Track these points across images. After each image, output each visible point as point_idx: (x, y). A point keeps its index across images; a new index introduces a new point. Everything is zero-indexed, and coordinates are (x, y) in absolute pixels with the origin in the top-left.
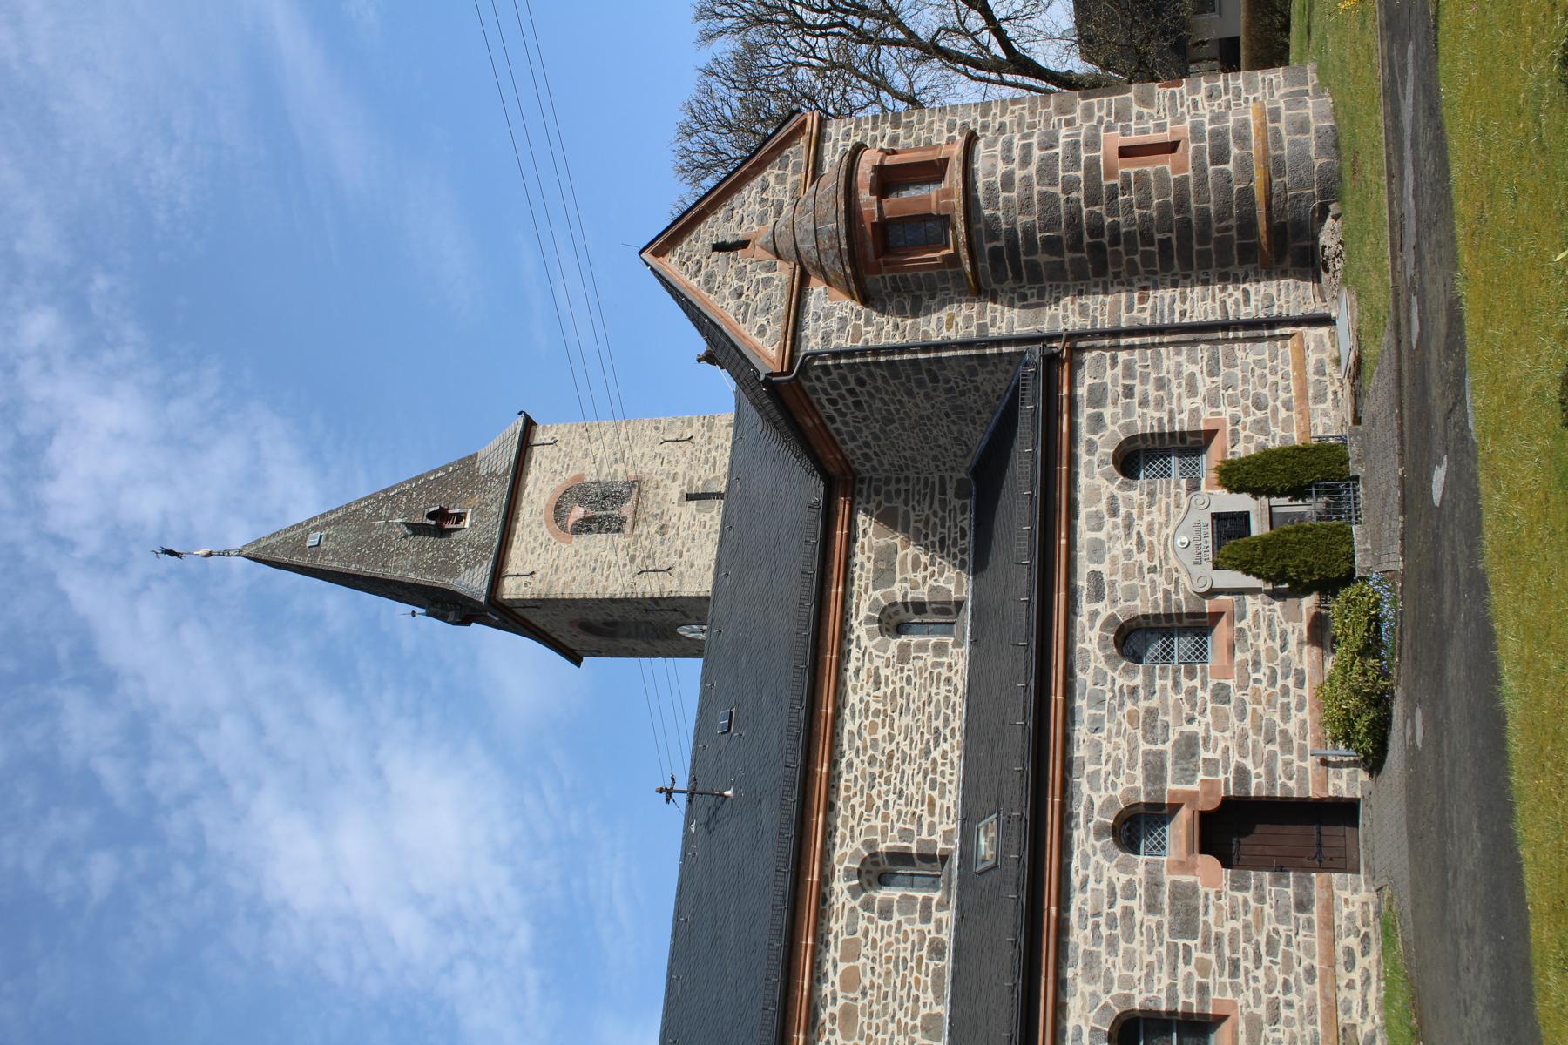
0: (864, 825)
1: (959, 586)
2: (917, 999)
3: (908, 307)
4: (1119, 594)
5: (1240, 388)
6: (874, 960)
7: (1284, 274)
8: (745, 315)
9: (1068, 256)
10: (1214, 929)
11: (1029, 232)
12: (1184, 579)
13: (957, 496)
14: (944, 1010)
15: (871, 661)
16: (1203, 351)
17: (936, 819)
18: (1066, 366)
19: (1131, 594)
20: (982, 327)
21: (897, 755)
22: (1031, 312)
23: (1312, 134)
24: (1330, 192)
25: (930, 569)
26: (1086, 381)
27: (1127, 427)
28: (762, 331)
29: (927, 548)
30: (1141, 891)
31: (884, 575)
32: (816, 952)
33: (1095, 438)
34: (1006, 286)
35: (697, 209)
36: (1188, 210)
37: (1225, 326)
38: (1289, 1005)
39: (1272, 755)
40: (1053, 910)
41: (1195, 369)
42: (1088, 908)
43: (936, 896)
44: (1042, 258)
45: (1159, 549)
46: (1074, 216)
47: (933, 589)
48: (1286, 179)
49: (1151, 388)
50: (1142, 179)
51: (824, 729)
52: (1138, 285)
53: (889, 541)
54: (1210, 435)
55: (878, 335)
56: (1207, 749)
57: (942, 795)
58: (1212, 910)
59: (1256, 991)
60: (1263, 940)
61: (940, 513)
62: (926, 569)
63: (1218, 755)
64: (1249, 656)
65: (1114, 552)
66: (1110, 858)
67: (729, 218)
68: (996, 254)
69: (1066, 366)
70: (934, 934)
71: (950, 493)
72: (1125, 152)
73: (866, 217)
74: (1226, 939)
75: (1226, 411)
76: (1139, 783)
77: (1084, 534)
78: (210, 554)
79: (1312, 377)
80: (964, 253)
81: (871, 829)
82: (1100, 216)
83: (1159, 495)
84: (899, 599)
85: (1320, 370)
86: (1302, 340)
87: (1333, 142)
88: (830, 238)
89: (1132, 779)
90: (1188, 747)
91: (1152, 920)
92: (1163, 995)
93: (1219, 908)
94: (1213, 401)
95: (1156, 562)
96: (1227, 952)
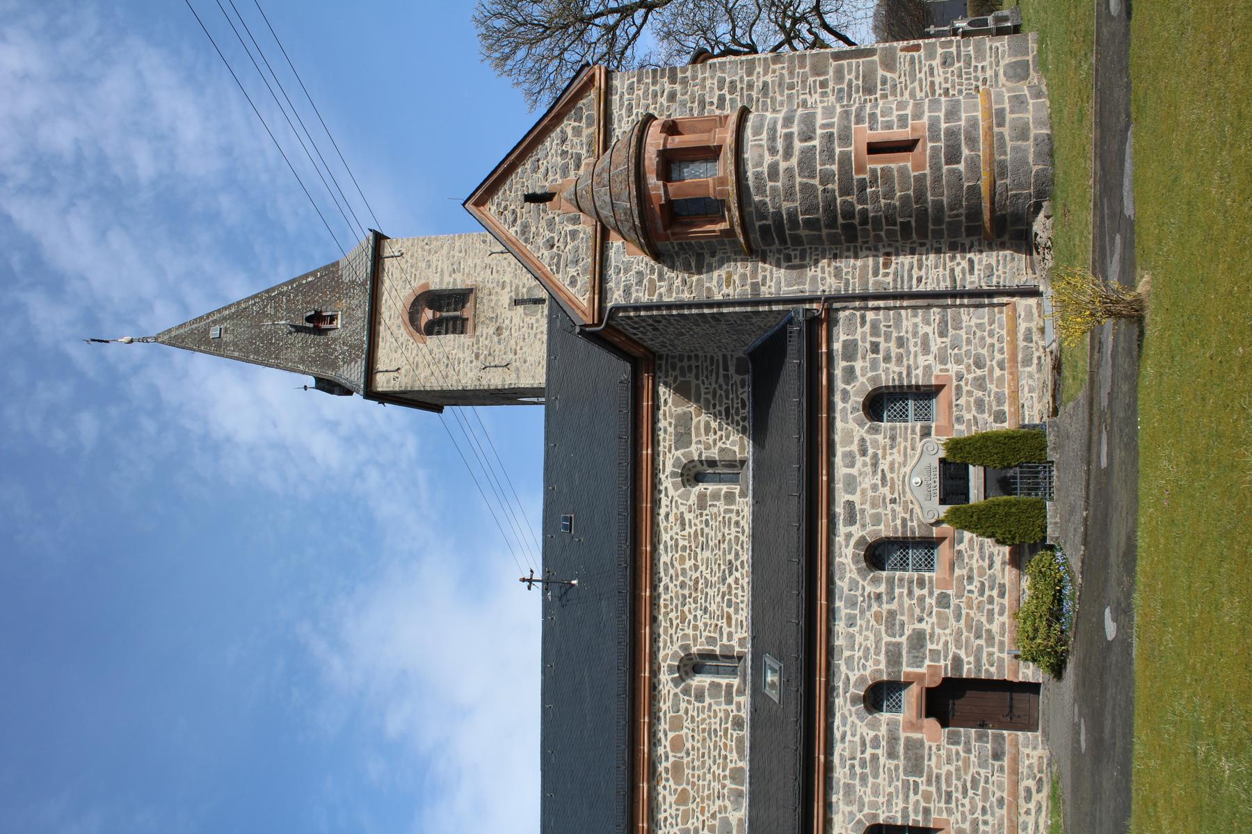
0: (680, 633)
1: (742, 448)
2: (725, 757)
3: (693, 264)
4: (868, 520)
5: (964, 348)
6: (693, 730)
7: (1003, 246)
8: (558, 268)
9: (824, 232)
10: (935, 771)
11: (792, 215)
12: (917, 510)
13: (738, 372)
14: (745, 765)
15: (677, 507)
16: (935, 314)
17: (733, 629)
18: (824, 326)
19: (877, 520)
20: (755, 286)
21: (701, 581)
22: (795, 273)
23: (1031, 142)
24: (1044, 191)
25: (719, 433)
26: (841, 337)
27: (875, 379)
28: (573, 282)
29: (715, 416)
30: (883, 743)
31: (683, 439)
32: (651, 725)
33: (848, 388)
34: (774, 248)
35: (508, 162)
36: (926, 201)
37: (954, 295)
38: (986, 823)
39: (980, 648)
40: (822, 757)
41: (929, 329)
42: (847, 754)
43: (736, 682)
44: (803, 232)
45: (898, 483)
46: (830, 205)
47: (722, 450)
48: (1008, 181)
49: (893, 345)
50: (887, 173)
51: (645, 563)
52: (882, 250)
53: (685, 409)
54: (939, 388)
55: (670, 290)
56: (932, 643)
57: (736, 611)
58: (934, 758)
59: (963, 813)
60: (969, 778)
61: (725, 387)
62: (715, 433)
63: (940, 647)
64: (965, 572)
65: (864, 486)
66: (862, 719)
67: (536, 169)
68: (765, 230)
69: (824, 326)
70: (735, 713)
71: (732, 370)
72: (874, 148)
73: (654, 200)
74: (943, 778)
75: (953, 368)
76: (882, 666)
77: (841, 470)
78: (131, 341)
79: (1021, 344)
80: (738, 230)
81: (685, 636)
82: (852, 204)
83: (898, 440)
84: (696, 458)
85: (1028, 338)
86: (1015, 310)
87: (1049, 150)
88: (625, 214)
89: (877, 662)
90: (918, 640)
91: (892, 764)
92: (899, 815)
93: (939, 757)
94: (943, 360)
95: (896, 495)
96: (944, 787)
